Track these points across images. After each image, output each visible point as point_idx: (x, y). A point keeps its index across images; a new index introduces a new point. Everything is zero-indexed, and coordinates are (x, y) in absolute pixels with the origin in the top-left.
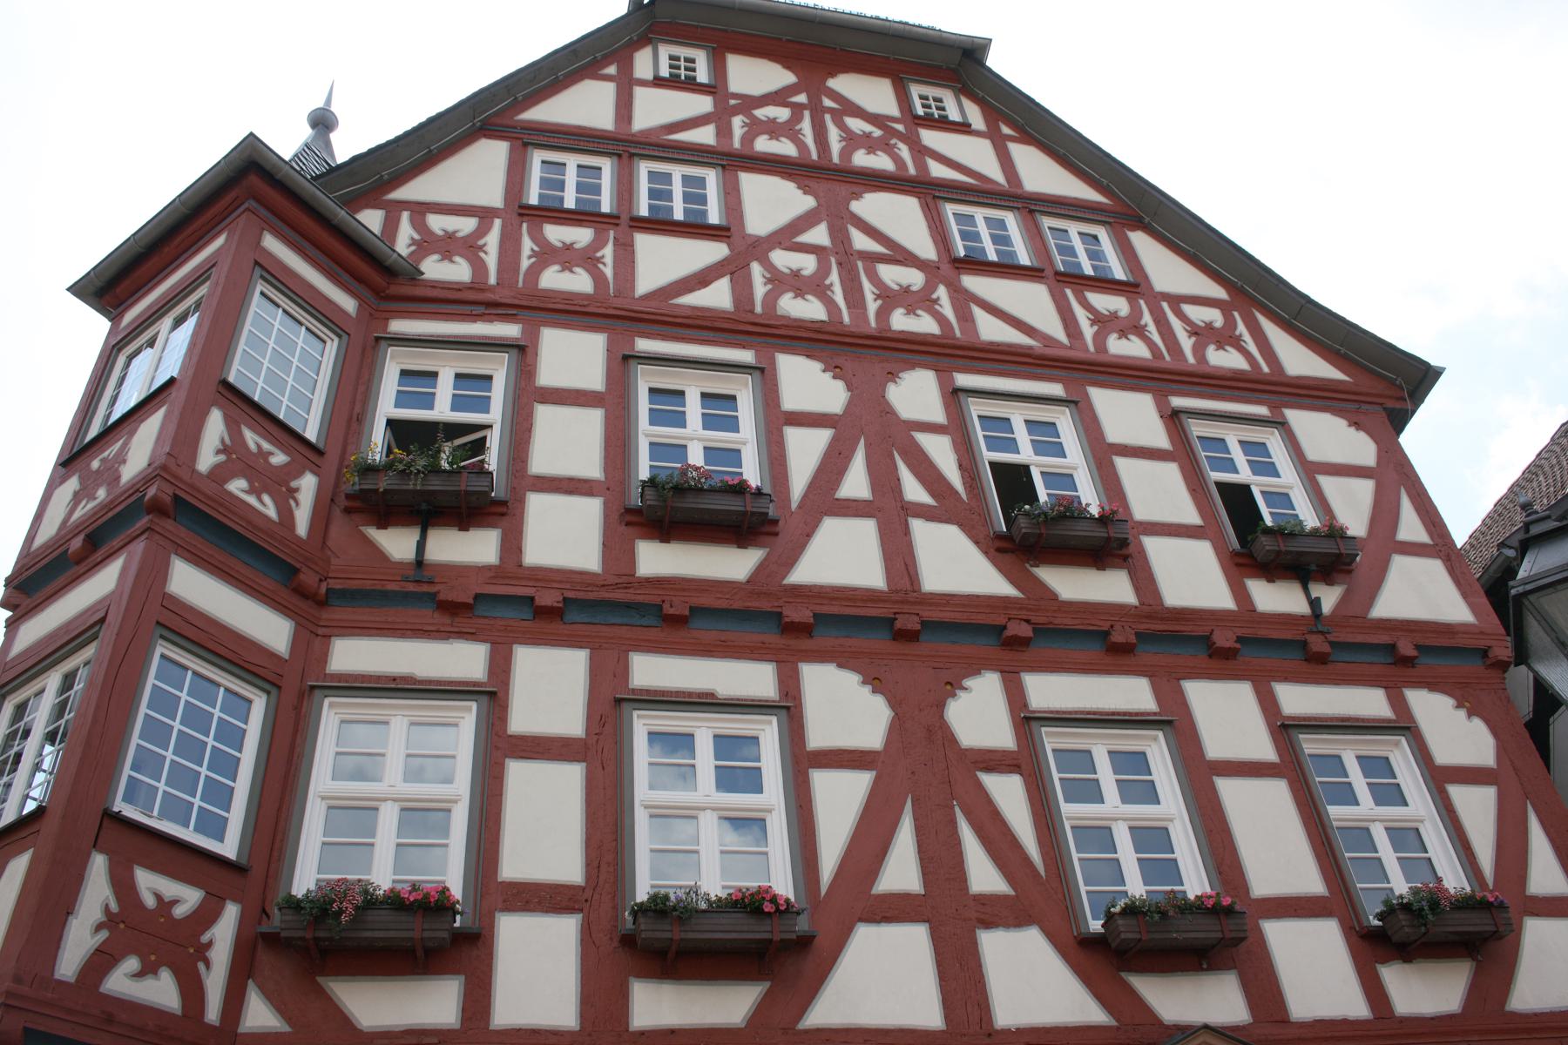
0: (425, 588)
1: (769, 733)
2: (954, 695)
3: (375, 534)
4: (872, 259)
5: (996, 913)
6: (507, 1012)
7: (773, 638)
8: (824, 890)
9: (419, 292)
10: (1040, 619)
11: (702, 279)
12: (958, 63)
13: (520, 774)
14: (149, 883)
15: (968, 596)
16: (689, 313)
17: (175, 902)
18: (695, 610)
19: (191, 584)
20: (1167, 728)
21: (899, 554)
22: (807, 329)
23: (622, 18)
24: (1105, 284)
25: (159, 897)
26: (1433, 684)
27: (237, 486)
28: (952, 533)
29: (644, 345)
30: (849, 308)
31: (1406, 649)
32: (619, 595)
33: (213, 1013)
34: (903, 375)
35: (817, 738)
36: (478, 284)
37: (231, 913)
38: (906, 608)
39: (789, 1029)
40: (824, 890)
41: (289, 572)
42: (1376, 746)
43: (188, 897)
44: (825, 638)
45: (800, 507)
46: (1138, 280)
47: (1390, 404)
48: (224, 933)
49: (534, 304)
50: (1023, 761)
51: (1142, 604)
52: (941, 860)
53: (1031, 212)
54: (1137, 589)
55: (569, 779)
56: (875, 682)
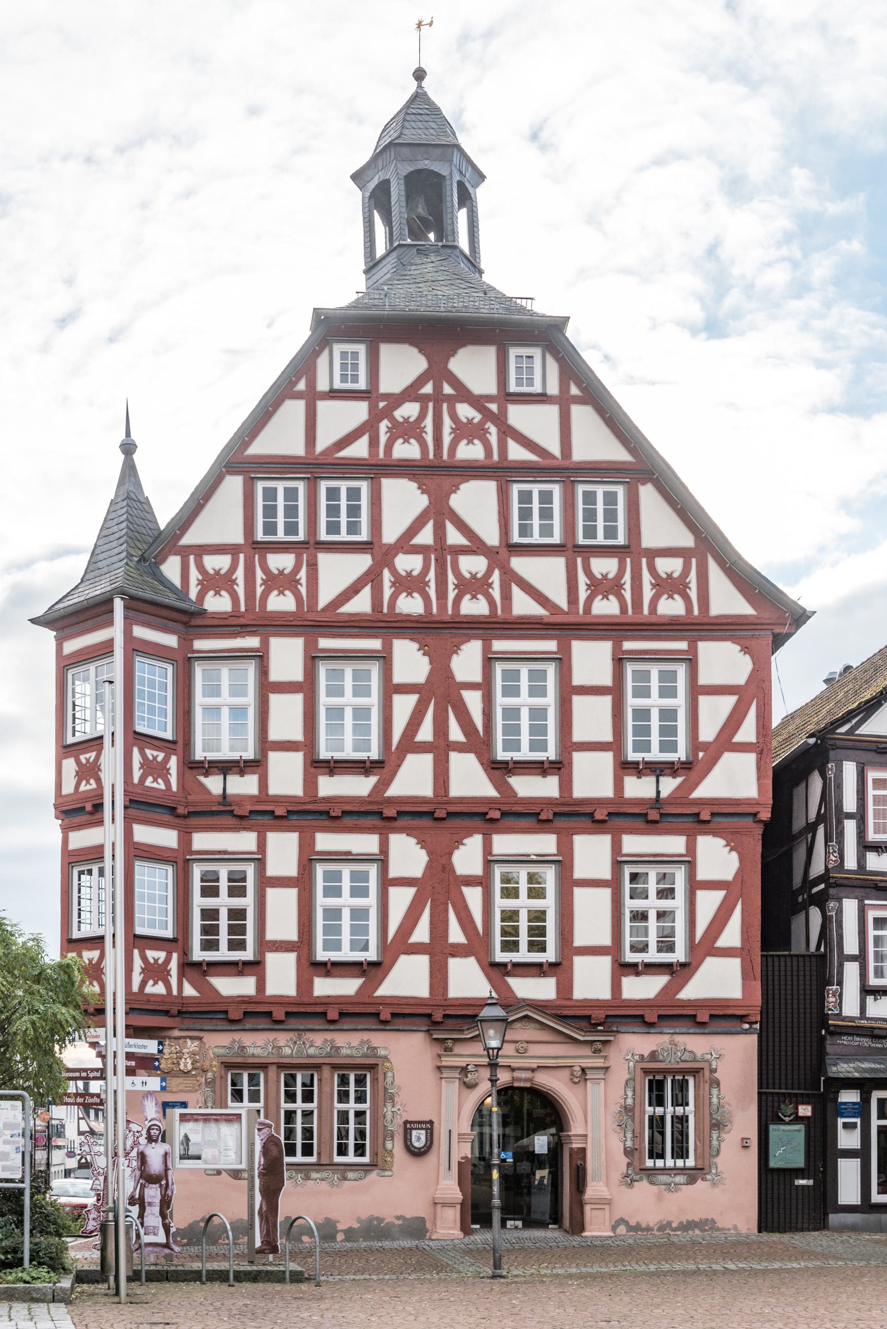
0: (228, 808)
1: (373, 870)
2: (458, 848)
3: (202, 779)
5: (458, 951)
6: (271, 990)
7: (377, 822)
8: (389, 942)
10: (506, 808)
11: (353, 590)
12: (548, 335)
13: (275, 699)
16: (347, 619)
18: (344, 813)
21: (439, 976)
22: (412, 621)
23: (310, 337)
26: (408, 831)
28: (471, 758)
29: (324, 643)
30: (437, 599)
33: (175, 992)
34: (463, 647)
36: (235, 613)
37: (175, 956)
38: (441, 806)
39: (371, 996)
40: (389, 942)
41: (172, 810)
43: (161, 955)
44: (403, 822)
45: (396, 749)
47: (777, 630)
48: (174, 966)
50: (484, 882)
51: (561, 797)
52: (439, 928)
55: (292, 894)
56: (422, 843)
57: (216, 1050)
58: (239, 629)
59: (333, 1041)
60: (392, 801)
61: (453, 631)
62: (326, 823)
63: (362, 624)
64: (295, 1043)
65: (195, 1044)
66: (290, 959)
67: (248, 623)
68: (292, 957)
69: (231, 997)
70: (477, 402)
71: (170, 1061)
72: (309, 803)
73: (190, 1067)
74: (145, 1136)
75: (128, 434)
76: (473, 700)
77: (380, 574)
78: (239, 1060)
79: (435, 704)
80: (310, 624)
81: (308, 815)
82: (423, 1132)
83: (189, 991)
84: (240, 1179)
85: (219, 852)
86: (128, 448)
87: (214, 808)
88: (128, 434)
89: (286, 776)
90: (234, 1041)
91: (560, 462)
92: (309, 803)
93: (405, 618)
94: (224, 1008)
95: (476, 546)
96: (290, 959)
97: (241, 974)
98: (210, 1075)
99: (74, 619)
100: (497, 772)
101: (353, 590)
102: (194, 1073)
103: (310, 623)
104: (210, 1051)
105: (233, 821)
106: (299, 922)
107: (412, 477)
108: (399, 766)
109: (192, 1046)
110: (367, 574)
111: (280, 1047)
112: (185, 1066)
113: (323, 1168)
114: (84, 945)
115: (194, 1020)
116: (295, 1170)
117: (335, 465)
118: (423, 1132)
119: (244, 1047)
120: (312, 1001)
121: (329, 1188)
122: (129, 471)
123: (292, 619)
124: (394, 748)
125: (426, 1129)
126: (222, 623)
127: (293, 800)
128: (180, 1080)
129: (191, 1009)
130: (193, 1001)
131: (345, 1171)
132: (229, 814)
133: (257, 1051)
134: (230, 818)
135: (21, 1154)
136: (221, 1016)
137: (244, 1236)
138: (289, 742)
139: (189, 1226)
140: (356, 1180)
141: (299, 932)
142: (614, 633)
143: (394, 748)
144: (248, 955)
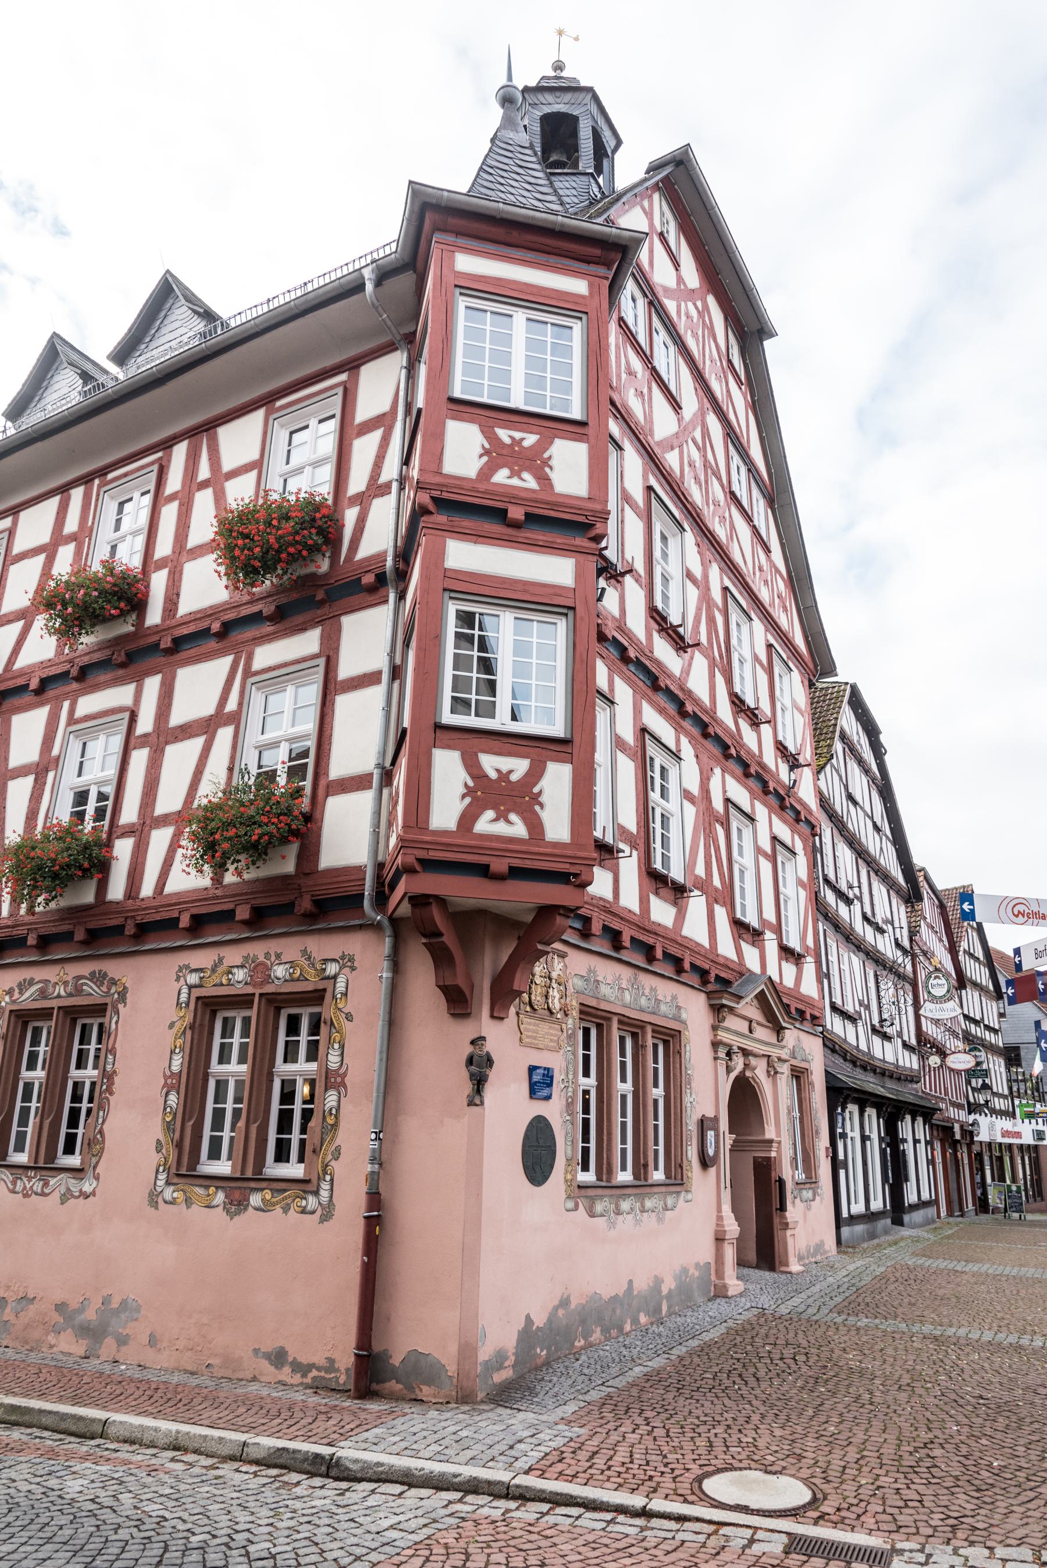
14: (491, 763)
17: (511, 772)
19: (464, 555)
25: (498, 771)
27: (502, 476)
43: (519, 767)
116: (635, 1195)
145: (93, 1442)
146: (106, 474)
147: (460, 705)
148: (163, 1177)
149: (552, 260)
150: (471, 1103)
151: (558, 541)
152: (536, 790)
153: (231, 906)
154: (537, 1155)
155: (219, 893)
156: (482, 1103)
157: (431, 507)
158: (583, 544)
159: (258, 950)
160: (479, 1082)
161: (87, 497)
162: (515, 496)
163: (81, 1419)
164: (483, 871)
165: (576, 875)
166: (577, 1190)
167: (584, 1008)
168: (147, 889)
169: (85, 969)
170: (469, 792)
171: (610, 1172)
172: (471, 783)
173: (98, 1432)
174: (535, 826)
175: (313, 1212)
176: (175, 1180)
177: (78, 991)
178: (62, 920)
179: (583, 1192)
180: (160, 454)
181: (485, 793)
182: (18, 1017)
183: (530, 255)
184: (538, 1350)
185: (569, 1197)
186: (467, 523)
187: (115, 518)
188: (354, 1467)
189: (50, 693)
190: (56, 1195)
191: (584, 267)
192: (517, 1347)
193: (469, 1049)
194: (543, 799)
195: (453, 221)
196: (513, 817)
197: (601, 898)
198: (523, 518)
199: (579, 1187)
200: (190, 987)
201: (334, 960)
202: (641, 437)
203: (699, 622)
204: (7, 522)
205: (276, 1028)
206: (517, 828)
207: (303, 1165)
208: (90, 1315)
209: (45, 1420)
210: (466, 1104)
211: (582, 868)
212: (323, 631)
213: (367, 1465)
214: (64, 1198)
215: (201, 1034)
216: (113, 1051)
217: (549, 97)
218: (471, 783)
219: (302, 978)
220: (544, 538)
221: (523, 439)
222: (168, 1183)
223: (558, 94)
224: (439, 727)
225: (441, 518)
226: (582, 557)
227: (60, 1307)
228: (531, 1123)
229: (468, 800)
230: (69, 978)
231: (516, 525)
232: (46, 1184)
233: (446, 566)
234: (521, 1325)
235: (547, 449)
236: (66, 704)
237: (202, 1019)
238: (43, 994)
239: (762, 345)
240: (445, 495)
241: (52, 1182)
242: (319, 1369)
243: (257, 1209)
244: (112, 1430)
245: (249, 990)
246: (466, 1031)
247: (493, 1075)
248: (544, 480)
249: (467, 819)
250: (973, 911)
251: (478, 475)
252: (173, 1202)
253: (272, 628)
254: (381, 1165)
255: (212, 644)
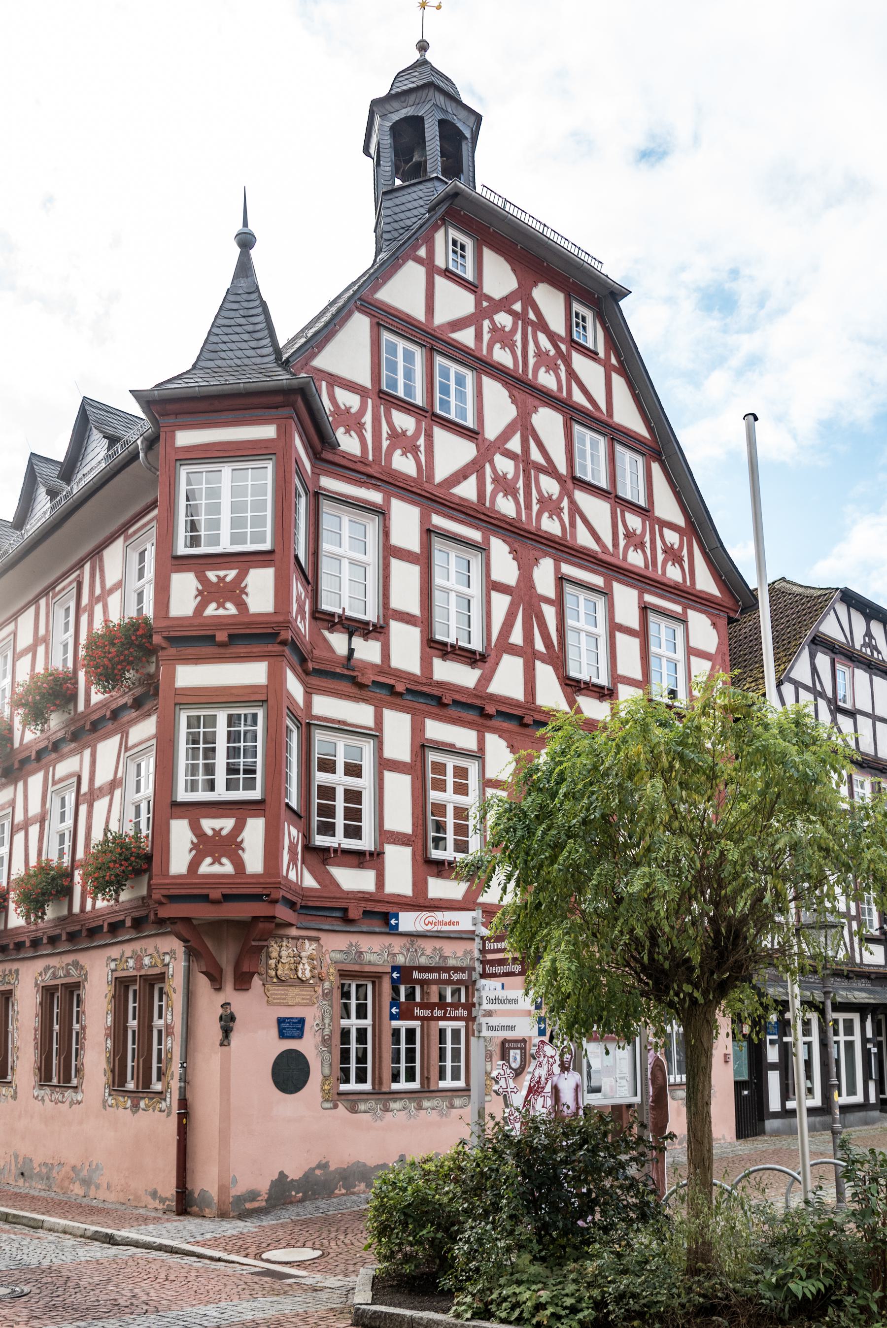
3: (326, 633)
4: (540, 469)
9: (337, 459)
14: (208, 825)
15: (409, 673)
16: (458, 501)
17: (221, 829)
20: (376, 739)
22: (507, 523)
24: (407, 407)
25: (213, 829)
26: (501, 733)
27: (211, 610)
31: (400, 688)
32: (425, 689)
35: (488, 775)
36: (363, 461)
38: (529, 712)
42: (462, 762)
43: (227, 824)
44: (497, 722)
46: (480, 431)
47: (732, 615)
49: (390, 480)
53: (432, 349)
54: (431, 664)
57: (333, 955)
58: (365, 478)
59: (441, 949)
60: (493, 698)
61: (534, 543)
62: (436, 710)
63: (469, 512)
64: (408, 950)
65: (313, 947)
66: (406, 852)
67: (375, 474)
68: (407, 851)
69: (352, 892)
70: (552, 337)
71: (287, 966)
72: (426, 684)
73: (308, 974)
74: (558, 1062)
75: (245, 224)
76: (549, 613)
77: (483, 467)
78: (356, 968)
79: (524, 610)
80: (429, 497)
81: (425, 698)
82: (518, 1051)
83: (309, 881)
84: (356, 1113)
85: (339, 722)
86: (246, 241)
87: (338, 670)
88: (245, 224)
89: (405, 650)
90: (351, 945)
91: (605, 418)
92: (426, 684)
93: (502, 518)
94: (344, 905)
95: (551, 470)
96: (406, 852)
97: (360, 865)
98: (327, 985)
99: (279, 399)
100: (569, 689)
101: (461, 476)
102: (311, 982)
103: (428, 495)
104: (327, 956)
105: (354, 690)
106: (413, 814)
107: (505, 384)
108: (497, 664)
109: (309, 948)
110: (474, 462)
111: (394, 955)
112: (303, 973)
113: (434, 1094)
114: (204, 810)
115: (309, 918)
116: (409, 1099)
117: (449, 344)
118: (518, 1051)
119: (361, 953)
120: (427, 904)
121: (438, 1118)
122: (244, 268)
123: (413, 484)
124: (493, 644)
125: (521, 1049)
126: (351, 466)
127: (412, 677)
128: (297, 991)
129: (310, 904)
130: (313, 894)
131: (452, 1097)
132: (349, 679)
133: (373, 958)
134: (349, 685)
135: (501, 1097)
136: (338, 914)
137: (360, 1182)
138: (408, 614)
139: (304, 1175)
140: (461, 1107)
141: (413, 825)
142: (639, 584)
143: (493, 644)
144: (366, 843)
145: (56, 1234)
146: (54, 588)
147: (192, 786)
148: (107, 1091)
149: (248, 413)
150: (222, 1045)
151: (255, 650)
152: (239, 840)
153: (122, 918)
154: (289, 1074)
155: (117, 908)
156: (229, 1044)
157: (164, 645)
158: (273, 649)
159: (137, 946)
160: (227, 1032)
161: (47, 605)
162: (219, 623)
163: (34, 1220)
164: (205, 898)
165: (267, 895)
166: (336, 1096)
167: (342, 972)
168: (89, 907)
169: (69, 959)
170: (195, 846)
171: (381, 1083)
172: (195, 841)
173: (36, 1226)
174: (239, 864)
175: (164, 1111)
176: (113, 1093)
177: (68, 974)
178: (56, 926)
179: (343, 1097)
180: (78, 573)
181: (207, 845)
182: (47, 990)
183: (230, 415)
184: (293, 1193)
185: (327, 1101)
186: (191, 651)
187: (138, 567)
188: (119, 1239)
189: (44, 761)
190: (67, 1103)
191: (273, 412)
192: (270, 1190)
193: (220, 1011)
194: (244, 845)
195: (170, 407)
196: (224, 860)
197: (359, 892)
198: (227, 639)
199: (338, 1094)
200: (113, 971)
201: (167, 953)
202: (414, 489)
203: (512, 626)
204: (10, 628)
205: (153, 997)
206: (227, 867)
207: (160, 1083)
208: (85, 1173)
209: (24, 1221)
210: (218, 1043)
211: (272, 890)
212: (158, 718)
213: (124, 1238)
214: (72, 1103)
215: (120, 1001)
216: (84, 1012)
217: (396, 104)
218: (195, 841)
219: (155, 966)
220: (245, 650)
221: (226, 576)
222: (110, 1095)
223: (403, 99)
224: (175, 804)
225: (172, 651)
226: (272, 659)
227: (74, 1168)
228: (302, 1054)
229: (194, 852)
230: (64, 965)
231: (222, 645)
232: (63, 1096)
233: (176, 686)
234: (276, 1176)
235: (243, 580)
236: (51, 769)
237: (120, 992)
238: (54, 976)
239: (618, 306)
240: (172, 634)
241: (66, 1094)
242: (169, 1200)
243: (143, 1110)
244: (45, 1225)
245: (135, 973)
246: (221, 998)
247: (237, 1026)
248: (242, 606)
249: (194, 865)
250: (397, 924)
251: (194, 613)
252: (111, 1106)
253: (135, 714)
254: (185, 1082)
255: (110, 726)
